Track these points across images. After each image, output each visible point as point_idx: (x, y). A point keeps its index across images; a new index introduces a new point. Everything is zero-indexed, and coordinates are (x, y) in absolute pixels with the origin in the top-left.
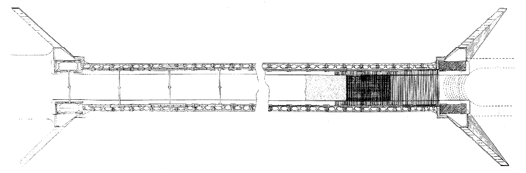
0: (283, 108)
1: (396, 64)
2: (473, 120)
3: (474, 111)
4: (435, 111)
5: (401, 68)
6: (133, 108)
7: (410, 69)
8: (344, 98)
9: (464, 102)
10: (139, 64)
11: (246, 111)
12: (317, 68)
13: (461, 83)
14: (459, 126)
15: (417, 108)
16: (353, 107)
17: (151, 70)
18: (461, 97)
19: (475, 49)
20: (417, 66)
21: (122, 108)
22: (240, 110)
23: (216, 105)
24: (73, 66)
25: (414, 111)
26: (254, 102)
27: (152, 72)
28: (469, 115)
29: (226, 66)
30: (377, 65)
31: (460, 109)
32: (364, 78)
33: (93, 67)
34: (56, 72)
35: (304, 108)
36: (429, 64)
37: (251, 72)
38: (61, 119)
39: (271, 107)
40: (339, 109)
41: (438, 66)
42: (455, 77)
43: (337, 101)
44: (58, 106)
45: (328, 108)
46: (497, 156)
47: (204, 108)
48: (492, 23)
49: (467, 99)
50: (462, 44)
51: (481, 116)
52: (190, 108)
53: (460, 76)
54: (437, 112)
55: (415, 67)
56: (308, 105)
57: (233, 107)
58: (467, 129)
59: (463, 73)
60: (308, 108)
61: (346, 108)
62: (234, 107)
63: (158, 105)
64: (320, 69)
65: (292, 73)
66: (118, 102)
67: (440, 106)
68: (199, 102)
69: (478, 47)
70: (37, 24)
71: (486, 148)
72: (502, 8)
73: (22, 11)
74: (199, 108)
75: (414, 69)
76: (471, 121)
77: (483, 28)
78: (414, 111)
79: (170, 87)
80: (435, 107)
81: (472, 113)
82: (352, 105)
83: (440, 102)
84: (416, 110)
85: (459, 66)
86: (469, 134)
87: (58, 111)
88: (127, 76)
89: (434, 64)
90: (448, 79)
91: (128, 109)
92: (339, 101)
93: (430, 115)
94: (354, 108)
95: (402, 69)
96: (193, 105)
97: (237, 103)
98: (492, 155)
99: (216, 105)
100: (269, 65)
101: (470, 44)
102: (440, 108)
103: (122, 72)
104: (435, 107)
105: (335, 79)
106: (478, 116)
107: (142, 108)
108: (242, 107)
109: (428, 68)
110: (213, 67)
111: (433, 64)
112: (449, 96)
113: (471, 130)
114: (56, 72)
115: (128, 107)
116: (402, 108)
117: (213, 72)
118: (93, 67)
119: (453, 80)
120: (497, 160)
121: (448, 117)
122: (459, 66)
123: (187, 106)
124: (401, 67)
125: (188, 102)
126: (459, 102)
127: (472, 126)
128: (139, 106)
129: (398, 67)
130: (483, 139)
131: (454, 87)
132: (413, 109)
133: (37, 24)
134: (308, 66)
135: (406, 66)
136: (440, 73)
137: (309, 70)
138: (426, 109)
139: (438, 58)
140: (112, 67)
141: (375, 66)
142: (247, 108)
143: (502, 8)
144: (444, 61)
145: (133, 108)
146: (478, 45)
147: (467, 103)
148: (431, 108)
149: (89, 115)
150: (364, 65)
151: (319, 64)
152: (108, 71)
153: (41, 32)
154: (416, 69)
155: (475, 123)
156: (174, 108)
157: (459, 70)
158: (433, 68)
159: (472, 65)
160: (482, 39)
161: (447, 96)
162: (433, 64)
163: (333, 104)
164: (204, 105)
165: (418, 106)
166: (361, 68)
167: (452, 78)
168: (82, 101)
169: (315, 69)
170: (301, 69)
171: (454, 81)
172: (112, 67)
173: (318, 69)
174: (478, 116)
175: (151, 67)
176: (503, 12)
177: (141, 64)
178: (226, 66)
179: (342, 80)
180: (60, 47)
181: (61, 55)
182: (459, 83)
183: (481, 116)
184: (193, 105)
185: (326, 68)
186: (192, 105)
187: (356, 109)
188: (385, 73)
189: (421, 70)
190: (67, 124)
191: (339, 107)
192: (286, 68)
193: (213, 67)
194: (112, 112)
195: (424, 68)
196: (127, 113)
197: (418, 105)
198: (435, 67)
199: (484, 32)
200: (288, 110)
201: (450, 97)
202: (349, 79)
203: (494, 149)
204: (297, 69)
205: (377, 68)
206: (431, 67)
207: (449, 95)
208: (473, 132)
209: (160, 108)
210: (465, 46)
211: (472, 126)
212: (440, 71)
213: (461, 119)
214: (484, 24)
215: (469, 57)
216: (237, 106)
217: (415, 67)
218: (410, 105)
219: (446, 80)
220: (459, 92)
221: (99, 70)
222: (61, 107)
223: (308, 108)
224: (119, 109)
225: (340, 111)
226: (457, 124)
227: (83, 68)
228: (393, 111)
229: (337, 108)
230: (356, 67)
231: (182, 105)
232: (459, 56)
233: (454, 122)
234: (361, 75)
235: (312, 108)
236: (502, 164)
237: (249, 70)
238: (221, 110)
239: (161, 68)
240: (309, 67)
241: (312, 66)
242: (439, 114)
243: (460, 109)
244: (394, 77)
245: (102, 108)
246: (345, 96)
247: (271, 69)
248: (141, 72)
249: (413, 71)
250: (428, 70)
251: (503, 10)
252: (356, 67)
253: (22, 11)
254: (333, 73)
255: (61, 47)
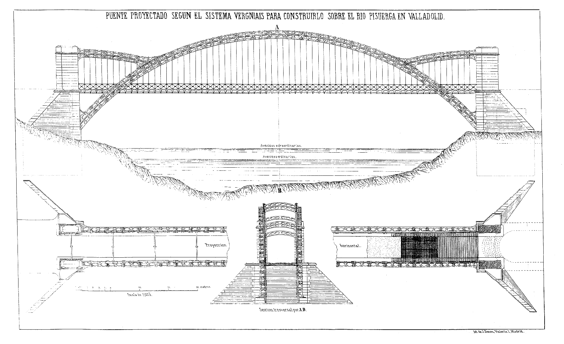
0: (349, 264)
1: (442, 228)
2: (506, 274)
3: (507, 266)
4: (475, 267)
5: (447, 231)
6: (124, 264)
7: (455, 231)
8: (399, 255)
9: (499, 259)
10: (213, 228)
11: (219, 266)
12: (377, 231)
13: (496, 243)
14: (495, 279)
15: (460, 264)
16: (407, 263)
17: (139, 232)
18: (496, 255)
19: (508, 214)
20: (460, 229)
21: (115, 264)
22: (213, 266)
23: (194, 262)
24: (75, 229)
25: (446, 267)
26: (225, 259)
27: (140, 234)
28: (503, 270)
29: (201, 229)
30: (426, 229)
31: (496, 265)
32: (417, 239)
33: (91, 230)
34: (60, 234)
35: (366, 264)
36: (470, 228)
37: (223, 234)
38: (64, 274)
39: (338, 263)
40: (395, 265)
41: (477, 229)
42: (492, 238)
43: (393, 258)
44: (62, 262)
45: (386, 264)
46: (527, 304)
47: (184, 264)
48: (523, 193)
49: (502, 257)
50: (497, 211)
51: (513, 271)
52: (172, 264)
53: (496, 237)
54: (476, 268)
55: (458, 230)
56: (353, 262)
57: (208, 263)
58: (501, 281)
59: (498, 235)
60: (369, 264)
61: (401, 264)
62: (208, 263)
63: (145, 261)
64: (379, 232)
65: (340, 234)
66: (112, 259)
67: (479, 262)
68: (180, 259)
69: (511, 214)
70: (45, 195)
71: (517, 297)
72: (531, 181)
73: (32, 183)
74: (179, 264)
75: (457, 231)
76: (505, 274)
77: (515, 197)
78: (446, 267)
79: (155, 246)
80: (475, 263)
81: (506, 269)
82: (405, 262)
83: (480, 259)
84: (459, 266)
85: (495, 229)
86: (503, 285)
87: (62, 266)
88: (120, 239)
89: (474, 227)
90: (498, 241)
91: (121, 264)
92: (395, 258)
93: (471, 270)
94: (393, 264)
95: (447, 231)
96: (174, 261)
97: (211, 259)
98: (522, 303)
99: (194, 262)
100: (337, 228)
101: (504, 211)
102: (479, 264)
103: (115, 234)
104: (475, 263)
105: (391, 239)
106: (511, 271)
107: (132, 264)
108: (132, 263)
109: (469, 231)
110: (191, 230)
111: (473, 227)
112: (487, 254)
113: (505, 282)
114: (60, 234)
115: (137, 263)
116: (392, 264)
117: (191, 234)
118: (91, 230)
119: (490, 240)
120: (527, 307)
121: (486, 272)
122: (495, 229)
123: (169, 262)
124: (447, 230)
125: (170, 259)
126: (495, 259)
127: (506, 279)
128: (130, 262)
129: (444, 229)
130: (515, 290)
131: (491, 246)
132: (456, 264)
133: (45, 195)
134: (369, 229)
135: (451, 229)
136: (479, 235)
137: (370, 232)
138: (468, 265)
139: (477, 222)
140: (107, 230)
141: (425, 229)
142: (187, 264)
143: (531, 181)
144: (483, 225)
145: (124, 264)
146: (511, 211)
147: (502, 259)
148: (472, 264)
149: (88, 270)
150: (416, 228)
151: (378, 228)
152: (104, 233)
153: (48, 200)
154: (459, 231)
155: (509, 277)
156: (158, 264)
157: (495, 232)
158: (473, 231)
159: (506, 228)
160: (514, 207)
161: (485, 254)
162: (473, 227)
163: (390, 260)
164: (183, 262)
165: (461, 262)
166: (413, 231)
167: (489, 239)
168: (82, 258)
169: (376, 231)
170: (363, 231)
171: (491, 242)
172: (107, 230)
173: (378, 231)
174: (511, 271)
175: (139, 229)
176: (532, 184)
177: (131, 227)
178: (202, 229)
179: (397, 241)
180: (64, 213)
181: (64, 220)
182: (495, 243)
183: (513, 271)
184: (174, 261)
185: (384, 230)
186: (173, 262)
187: (409, 264)
188: (433, 235)
189: (463, 233)
190: (70, 277)
191: (395, 263)
192: (351, 230)
193: (191, 230)
194: (400, 268)
195: (466, 231)
196: (120, 269)
197: (461, 262)
198: (475, 230)
199: (516, 200)
200: (352, 266)
201: (488, 255)
202: (404, 240)
203: (524, 298)
204: (360, 231)
205: (427, 231)
206: (471, 229)
207: (487, 253)
208: (506, 283)
209: (147, 264)
210: (500, 212)
211: (506, 279)
212: (479, 233)
213: (496, 273)
214: (516, 194)
215: (503, 221)
216: (211, 262)
217: (458, 230)
218: (454, 262)
219: (484, 241)
220: (495, 251)
221: (96, 232)
222: (64, 263)
223: (369, 264)
224: (113, 265)
225: (396, 267)
226: (493, 277)
227: (83, 231)
228: (440, 266)
229: (393, 264)
230: (410, 230)
231: (165, 261)
232: (495, 221)
233: (491, 275)
234: (413, 237)
235: (372, 264)
236: (531, 310)
237: (221, 232)
238: (197, 266)
239: (148, 230)
240: (370, 230)
241: (373, 229)
242: (478, 268)
243: (496, 265)
244: (469, 239)
245: (99, 264)
246: (400, 255)
247: (339, 231)
248: (131, 234)
249: (457, 233)
250: (469, 232)
251: (532, 182)
252: (410, 230)
253: (32, 183)
254: (390, 235)
255: (65, 213)
